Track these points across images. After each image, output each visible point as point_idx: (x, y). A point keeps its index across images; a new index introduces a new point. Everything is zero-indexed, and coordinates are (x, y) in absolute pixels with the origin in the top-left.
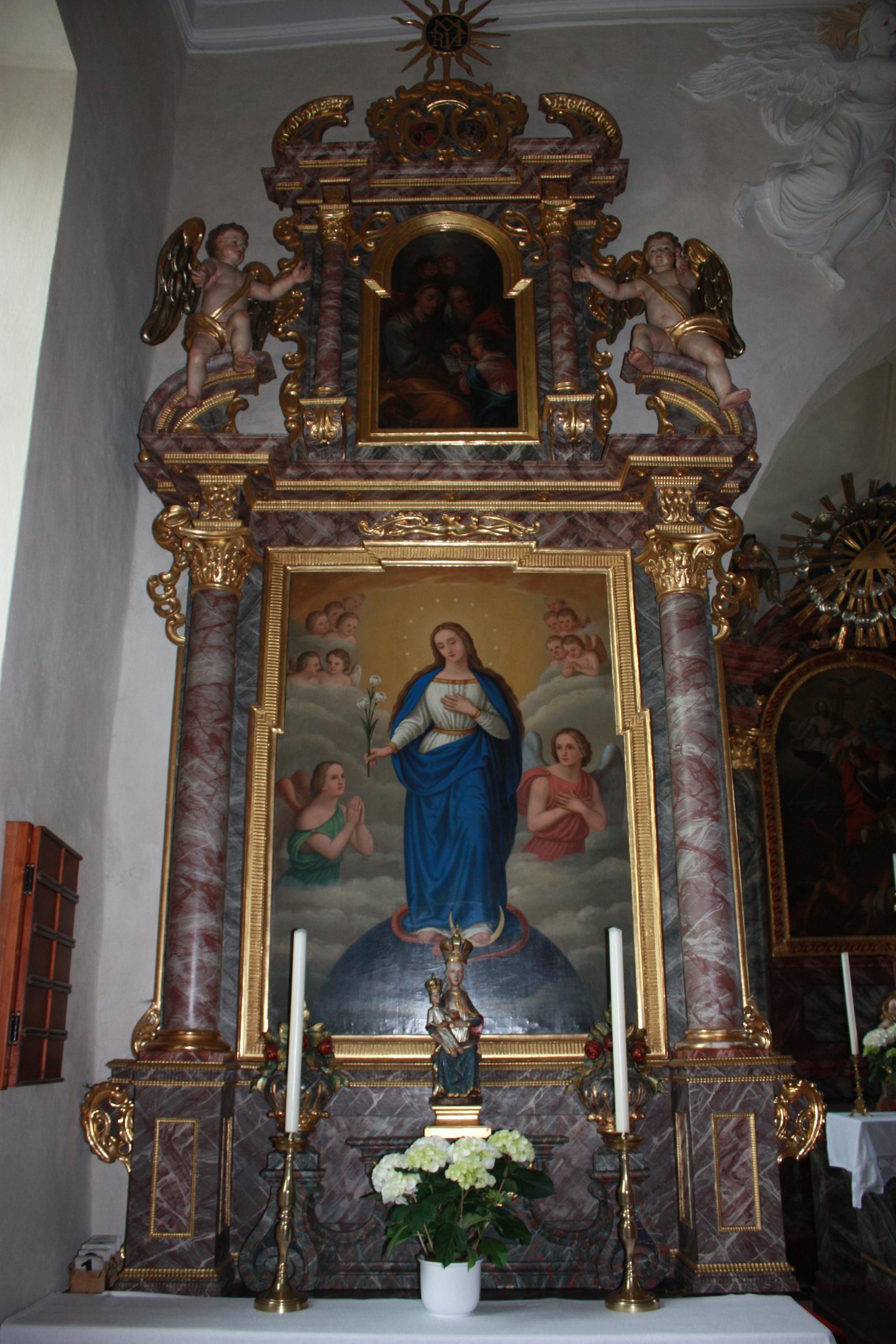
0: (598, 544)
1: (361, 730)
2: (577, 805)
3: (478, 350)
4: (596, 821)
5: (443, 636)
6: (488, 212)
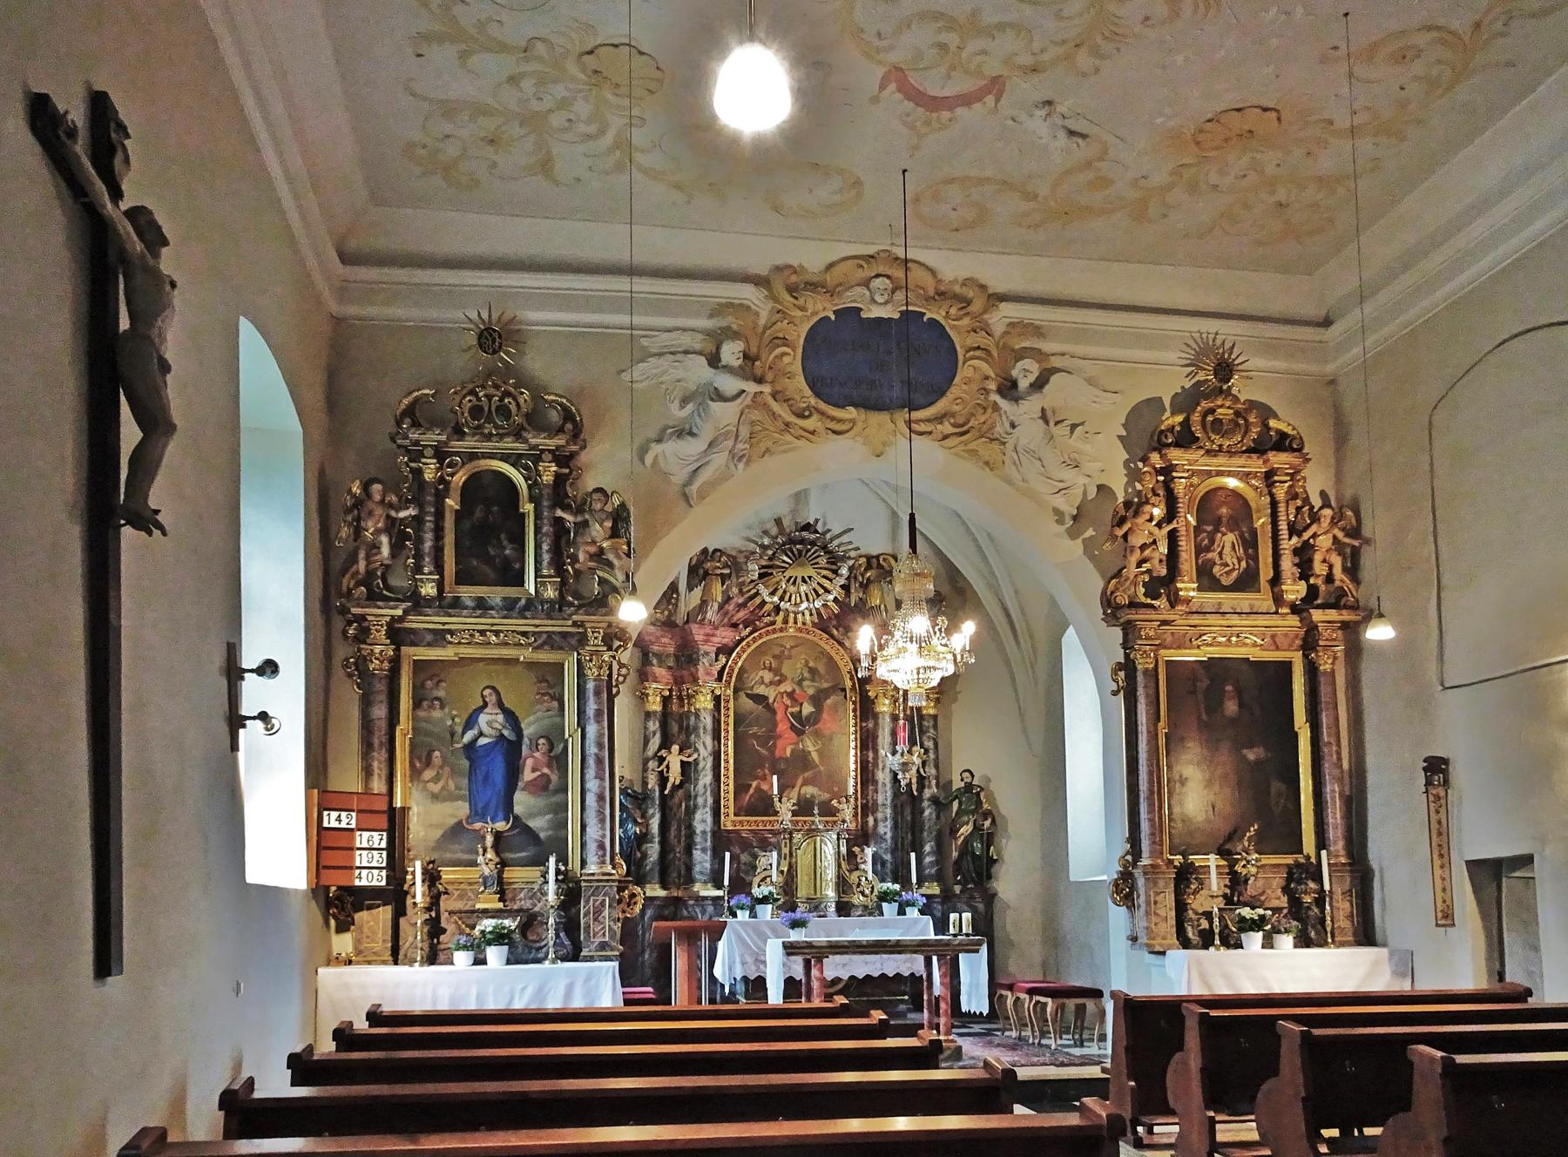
0: (561, 648)
1: (448, 736)
2: (546, 770)
3: (505, 543)
4: (554, 778)
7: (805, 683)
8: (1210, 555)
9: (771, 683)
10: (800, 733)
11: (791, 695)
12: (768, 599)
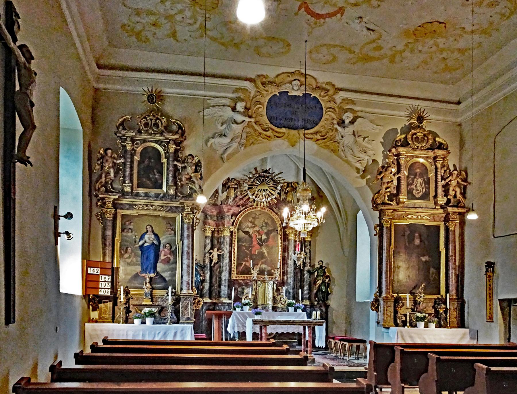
0: (175, 212)
1: (134, 243)
2: (169, 256)
3: (156, 173)
4: (172, 258)
5: (148, 227)
6: (159, 143)
7: (264, 228)
8: (412, 186)
9: (251, 227)
10: (261, 245)
11: (258, 232)
12: (251, 197)
